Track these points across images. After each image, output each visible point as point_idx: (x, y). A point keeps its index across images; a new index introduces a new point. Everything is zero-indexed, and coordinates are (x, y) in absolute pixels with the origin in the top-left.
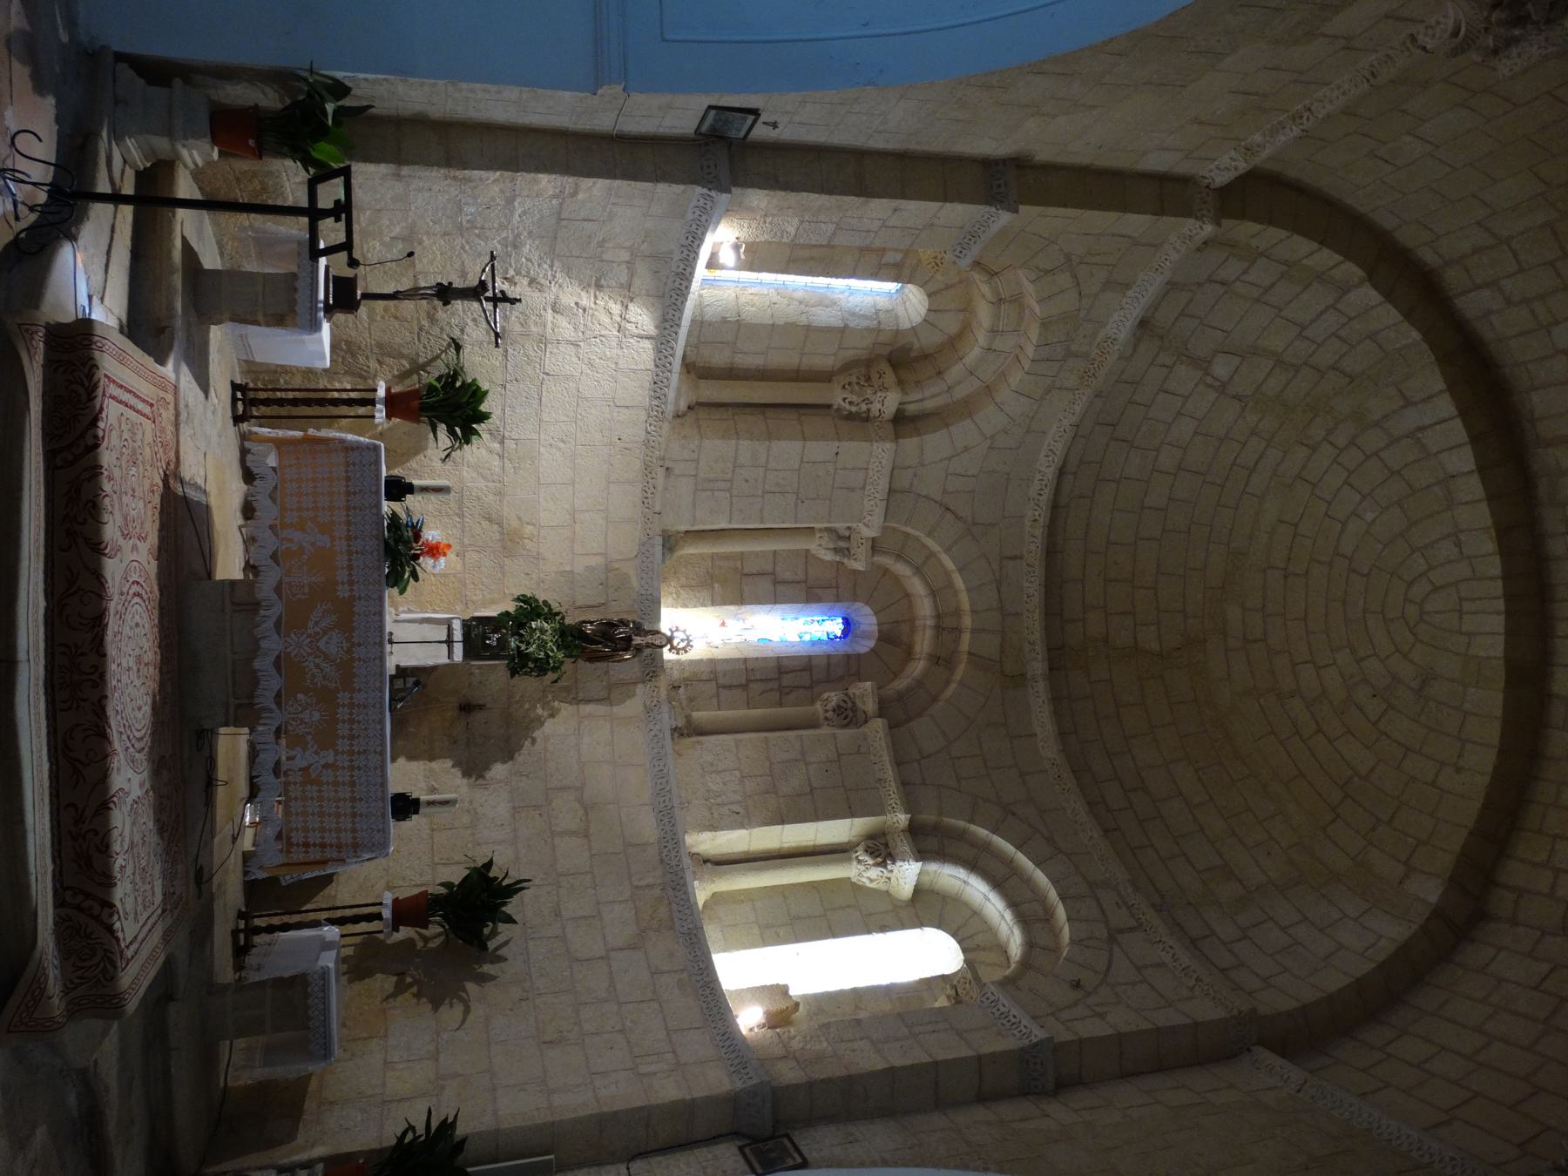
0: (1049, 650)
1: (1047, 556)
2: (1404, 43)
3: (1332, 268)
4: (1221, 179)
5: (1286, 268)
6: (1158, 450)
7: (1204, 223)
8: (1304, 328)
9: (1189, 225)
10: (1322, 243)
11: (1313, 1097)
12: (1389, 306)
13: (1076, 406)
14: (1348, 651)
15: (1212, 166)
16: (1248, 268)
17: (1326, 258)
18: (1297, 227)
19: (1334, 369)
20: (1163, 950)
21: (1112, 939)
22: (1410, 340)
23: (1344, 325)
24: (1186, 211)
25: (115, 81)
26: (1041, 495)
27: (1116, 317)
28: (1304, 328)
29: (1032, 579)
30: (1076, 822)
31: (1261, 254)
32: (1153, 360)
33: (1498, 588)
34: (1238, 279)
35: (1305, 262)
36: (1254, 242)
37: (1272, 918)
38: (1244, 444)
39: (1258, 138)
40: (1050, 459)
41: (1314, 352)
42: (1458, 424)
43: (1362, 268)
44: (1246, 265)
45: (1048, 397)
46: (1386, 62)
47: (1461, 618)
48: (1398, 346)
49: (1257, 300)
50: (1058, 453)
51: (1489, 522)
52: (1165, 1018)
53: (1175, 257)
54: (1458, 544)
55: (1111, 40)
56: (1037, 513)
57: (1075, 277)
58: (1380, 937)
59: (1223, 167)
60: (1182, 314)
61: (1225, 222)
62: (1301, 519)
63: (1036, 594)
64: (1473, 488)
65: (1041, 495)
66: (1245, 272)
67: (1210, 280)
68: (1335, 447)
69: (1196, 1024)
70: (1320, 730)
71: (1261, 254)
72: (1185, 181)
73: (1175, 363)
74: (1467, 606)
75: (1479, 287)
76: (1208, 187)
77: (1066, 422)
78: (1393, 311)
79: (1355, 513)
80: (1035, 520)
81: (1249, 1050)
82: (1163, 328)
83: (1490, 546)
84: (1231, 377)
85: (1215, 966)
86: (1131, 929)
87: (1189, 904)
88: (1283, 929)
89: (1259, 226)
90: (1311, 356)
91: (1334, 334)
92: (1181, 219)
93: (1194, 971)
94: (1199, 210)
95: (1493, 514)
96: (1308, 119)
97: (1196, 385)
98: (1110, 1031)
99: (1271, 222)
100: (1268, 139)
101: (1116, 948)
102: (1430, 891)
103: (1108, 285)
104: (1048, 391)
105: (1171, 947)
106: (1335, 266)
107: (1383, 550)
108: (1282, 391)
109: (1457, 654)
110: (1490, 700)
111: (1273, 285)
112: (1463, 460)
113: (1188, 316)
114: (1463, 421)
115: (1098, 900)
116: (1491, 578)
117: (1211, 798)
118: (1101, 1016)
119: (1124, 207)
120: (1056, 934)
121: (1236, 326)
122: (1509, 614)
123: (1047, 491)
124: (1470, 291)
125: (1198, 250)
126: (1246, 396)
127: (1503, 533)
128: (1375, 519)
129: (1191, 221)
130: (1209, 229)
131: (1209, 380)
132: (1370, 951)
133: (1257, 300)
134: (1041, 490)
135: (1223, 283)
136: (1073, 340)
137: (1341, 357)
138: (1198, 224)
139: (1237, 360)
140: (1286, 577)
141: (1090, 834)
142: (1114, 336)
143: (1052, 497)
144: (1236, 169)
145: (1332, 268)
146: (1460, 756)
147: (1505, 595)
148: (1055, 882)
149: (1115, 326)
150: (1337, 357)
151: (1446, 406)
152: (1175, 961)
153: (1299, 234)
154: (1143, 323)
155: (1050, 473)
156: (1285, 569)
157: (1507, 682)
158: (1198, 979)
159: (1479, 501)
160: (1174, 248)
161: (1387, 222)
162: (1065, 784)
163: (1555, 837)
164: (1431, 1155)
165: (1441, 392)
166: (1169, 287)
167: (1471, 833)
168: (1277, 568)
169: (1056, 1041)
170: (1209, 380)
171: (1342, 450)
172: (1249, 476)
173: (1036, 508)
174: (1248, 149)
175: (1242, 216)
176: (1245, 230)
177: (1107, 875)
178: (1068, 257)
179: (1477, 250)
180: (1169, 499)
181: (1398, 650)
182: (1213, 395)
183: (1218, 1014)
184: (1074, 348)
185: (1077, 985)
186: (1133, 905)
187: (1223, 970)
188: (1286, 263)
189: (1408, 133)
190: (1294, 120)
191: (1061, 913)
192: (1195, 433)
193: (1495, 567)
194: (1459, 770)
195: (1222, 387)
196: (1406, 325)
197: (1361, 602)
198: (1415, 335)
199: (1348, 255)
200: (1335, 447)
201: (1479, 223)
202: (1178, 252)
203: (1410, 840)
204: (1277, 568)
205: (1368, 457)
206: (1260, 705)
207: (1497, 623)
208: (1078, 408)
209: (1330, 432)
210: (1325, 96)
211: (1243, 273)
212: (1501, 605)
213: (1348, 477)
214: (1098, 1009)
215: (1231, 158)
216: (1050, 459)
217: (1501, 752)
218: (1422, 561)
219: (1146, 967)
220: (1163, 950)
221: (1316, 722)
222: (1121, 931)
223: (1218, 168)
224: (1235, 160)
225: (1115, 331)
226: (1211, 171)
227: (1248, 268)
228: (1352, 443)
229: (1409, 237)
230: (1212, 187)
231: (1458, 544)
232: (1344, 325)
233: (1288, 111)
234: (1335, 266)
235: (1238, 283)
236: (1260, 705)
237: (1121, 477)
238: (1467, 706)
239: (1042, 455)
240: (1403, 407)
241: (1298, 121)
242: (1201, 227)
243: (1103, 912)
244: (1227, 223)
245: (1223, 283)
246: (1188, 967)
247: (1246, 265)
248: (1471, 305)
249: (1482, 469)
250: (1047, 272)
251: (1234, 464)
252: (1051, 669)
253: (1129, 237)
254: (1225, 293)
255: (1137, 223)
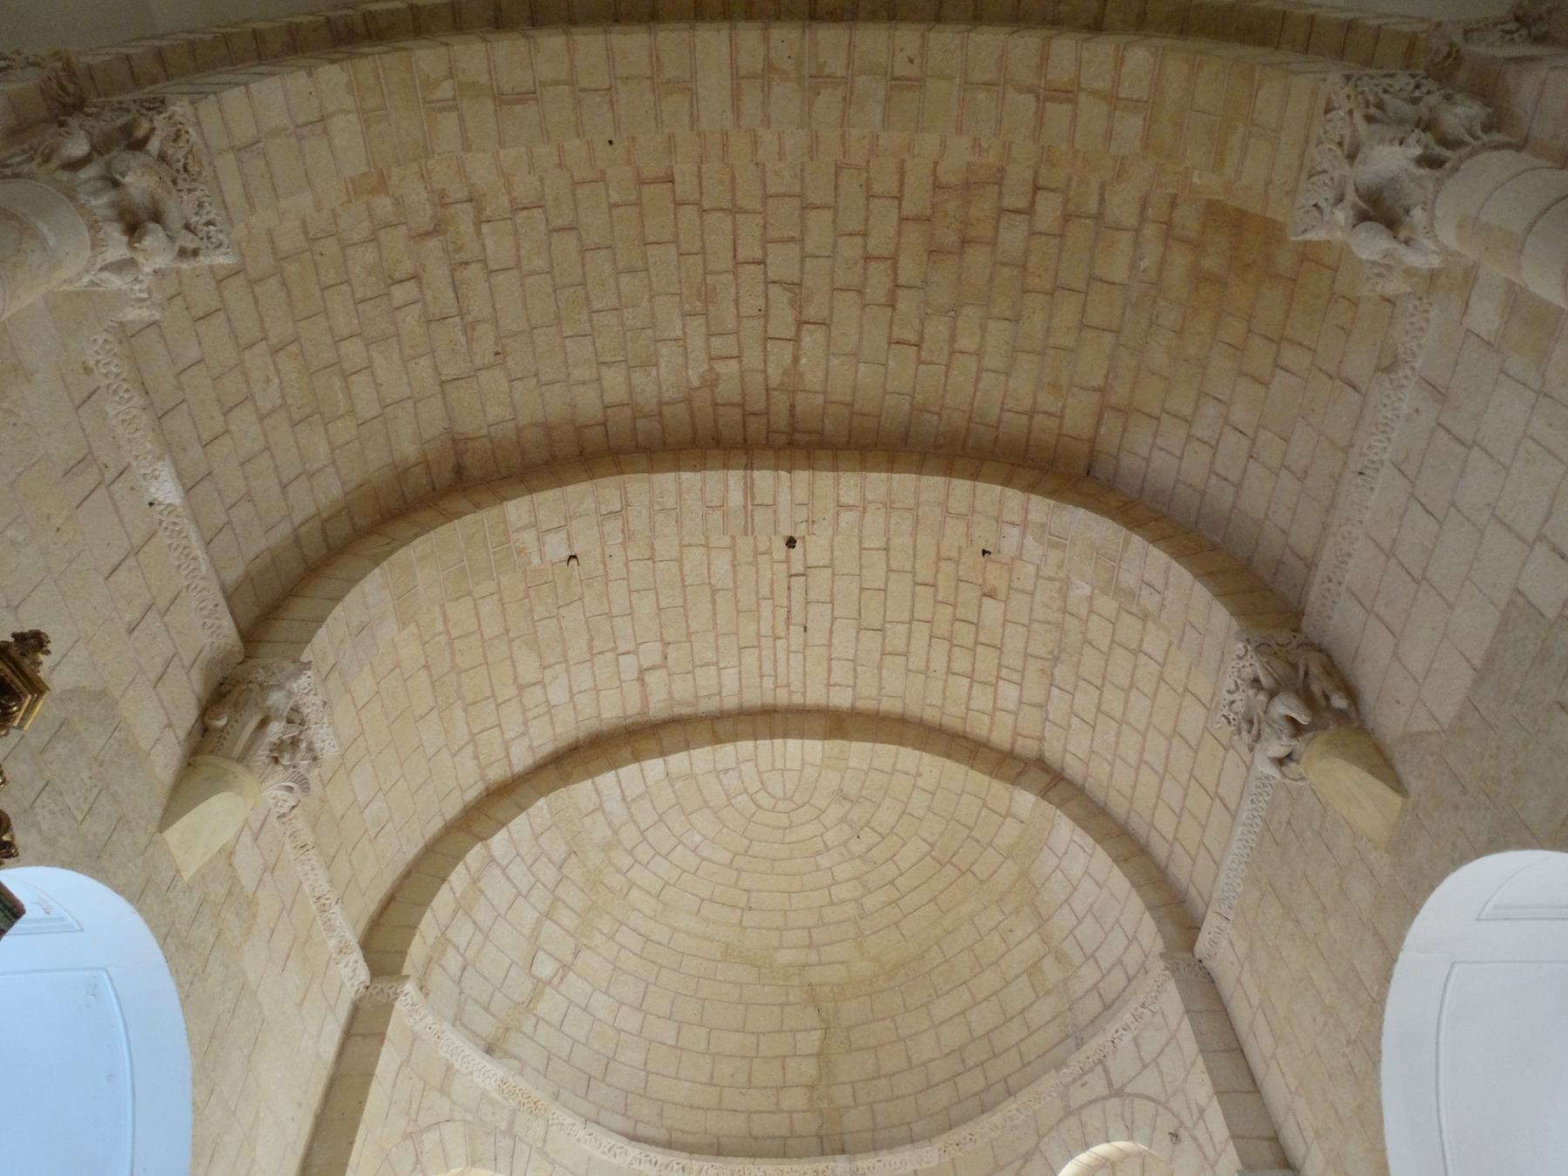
0: (823, 1153)
1: (722, 1155)
2: (284, 823)
3: (469, 871)
4: (363, 974)
5: (461, 911)
6: (619, 1031)
7: (402, 992)
8: (519, 894)
9: (400, 1006)
10: (444, 880)
11: (1230, 908)
12: (511, 824)
13: (566, 1122)
14: (818, 858)
15: (348, 984)
16: (454, 946)
17: (458, 876)
18: (424, 903)
19: (561, 867)
20: (1121, 1040)
21: (1119, 1093)
22: (545, 807)
23: (523, 860)
24: (387, 1009)
25: (1487, 903)
26: (656, 1163)
27: (478, 1080)
28: (519, 894)
29: (747, 1172)
30: (1003, 1127)
31: (443, 934)
32: (528, 1037)
33: (764, 744)
34: (462, 955)
35: (458, 895)
36: (431, 941)
37: (1071, 931)
38: (622, 946)
39: (332, 943)
40: (618, 1151)
41: (543, 884)
42: (623, 771)
43: (473, 847)
44: (450, 948)
45: (552, 1156)
46: (296, 837)
47: (789, 770)
48: (548, 816)
49: (486, 937)
50: (614, 1142)
51: (709, 748)
52: (1191, 1047)
53: (430, 1019)
54: (726, 771)
55: (194, 1103)
56: (676, 1167)
57: (429, 1128)
58: (1072, 840)
59: (353, 973)
60: (487, 1009)
61: (405, 972)
62: (696, 895)
63: (763, 1168)
64: (678, 761)
65: (656, 1163)
66: (457, 948)
67: (459, 982)
68: (633, 865)
69: (1188, 1011)
70: (892, 883)
71: (443, 934)
72: (356, 1009)
73: (535, 1015)
74: (779, 765)
75: (507, 755)
76: (367, 987)
77: (581, 1134)
78: (517, 820)
79: (694, 851)
80: (683, 1168)
81: (1200, 961)
82: (498, 1028)
83: (728, 748)
84: (556, 959)
85: (1126, 987)
86: (1106, 1072)
87: (1070, 1009)
88: (1080, 921)
89: (417, 937)
90: (546, 887)
91: (529, 868)
92: (394, 1013)
93: (1136, 1010)
94: (389, 996)
95: (701, 746)
96: (327, 899)
97: (560, 993)
98: (1215, 1102)
99: (414, 927)
100: (335, 933)
101: (1129, 1089)
102: (1025, 801)
103: (444, 1091)
104: (545, 1155)
105: (1117, 1031)
106: (467, 868)
107: (728, 827)
108: (574, 911)
109: (820, 773)
110: (858, 752)
111: (474, 922)
112: (654, 767)
113: (489, 1005)
114: (621, 766)
115: (1082, 1107)
116: (756, 747)
117: (964, 983)
118: (1202, 1112)
119: (368, 1076)
120: (1126, 1156)
121: (507, 956)
122: (785, 736)
123: (652, 1155)
124: (510, 761)
125: (427, 995)
126: (576, 945)
127: (717, 739)
128: (701, 834)
129: (397, 1004)
130: (409, 987)
131: (555, 981)
132: (1087, 850)
133: (486, 937)
134: (651, 1162)
135: (464, 969)
136: (496, 1128)
137: (551, 861)
138: (402, 998)
139: (541, 955)
140: (750, 909)
141: (1014, 1112)
142: (499, 1082)
143: (659, 1149)
144: (356, 962)
145: (469, 871)
146: (907, 773)
147: (771, 738)
148: (1070, 1156)
149: (487, 1081)
150: (550, 865)
151: (606, 780)
152: (1130, 1028)
153: (431, 901)
154: (489, 1050)
155: (634, 1151)
156: (743, 910)
157: (843, 738)
158: (1143, 1005)
159: (690, 756)
160: (421, 1020)
161: (436, 825)
162: (965, 1138)
163: (967, 708)
164: (1254, 817)
165: (593, 783)
166: (458, 1023)
167: (972, 767)
168: (742, 916)
169: (1241, 1167)
170: (555, 981)
171: (636, 861)
172: (652, 941)
173: (669, 1169)
174: (341, 951)
175: (403, 953)
176: (417, 950)
177: (1055, 1095)
178: (407, 1136)
179: (476, 757)
180: (669, 1019)
181: (818, 817)
182: (571, 977)
183: (1172, 991)
184: (503, 1126)
185: (1175, 1136)
186: (1081, 1068)
187: (1129, 980)
188: (455, 912)
189: (362, 813)
190: (324, 911)
191: (1101, 1149)
192: (606, 993)
193: (746, 746)
194: (919, 774)
195: (565, 968)
196: (531, 810)
197: (776, 846)
198: (541, 802)
199: (459, 858)
200: (633, 865)
201: (454, 756)
202: (425, 1017)
203: (983, 813)
204: (742, 916)
205: (645, 839)
206: (872, 934)
207: (793, 744)
208: (568, 1120)
209: (618, 871)
210: (311, 885)
211: (458, 951)
212: (778, 742)
213: (660, 855)
214: (1196, 1115)
215: (346, 966)
216: (618, 1151)
217: (902, 744)
218: (739, 798)
219: (1142, 1060)
220: (1121, 1040)
221: (884, 885)
222: (1110, 1084)
223: (351, 979)
224: (348, 963)
225: (493, 1080)
226: (352, 985)
227: (454, 946)
228: (630, 852)
229: (453, 808)
230: (368, 984)
231: (726, 771)
232: (523, 860)
233: (314, 919)
234: (467, 868)
235: (471, 927)
236: (872, 934)
237: (644, 1070)
238: (865, 767)
239: (614, 1161)
240: (603, 812)
241: (326, 908)
242: (406, 995)
243: (1095, 1101)
244: (407, 969)
245: (464, 969)
246: (1133, 1015)
247: (450, 948)
248: (522, 759)
249: (663, 753)
250: (418, 1161)
251: (641, 957)
252: (843, 1151)
253: (399, 1069)
254: (474, 967)
255: (388, 1060)
